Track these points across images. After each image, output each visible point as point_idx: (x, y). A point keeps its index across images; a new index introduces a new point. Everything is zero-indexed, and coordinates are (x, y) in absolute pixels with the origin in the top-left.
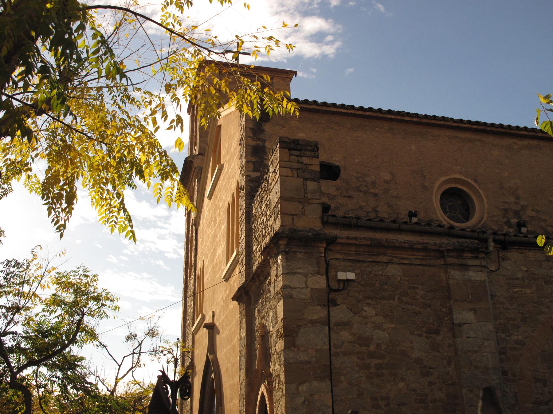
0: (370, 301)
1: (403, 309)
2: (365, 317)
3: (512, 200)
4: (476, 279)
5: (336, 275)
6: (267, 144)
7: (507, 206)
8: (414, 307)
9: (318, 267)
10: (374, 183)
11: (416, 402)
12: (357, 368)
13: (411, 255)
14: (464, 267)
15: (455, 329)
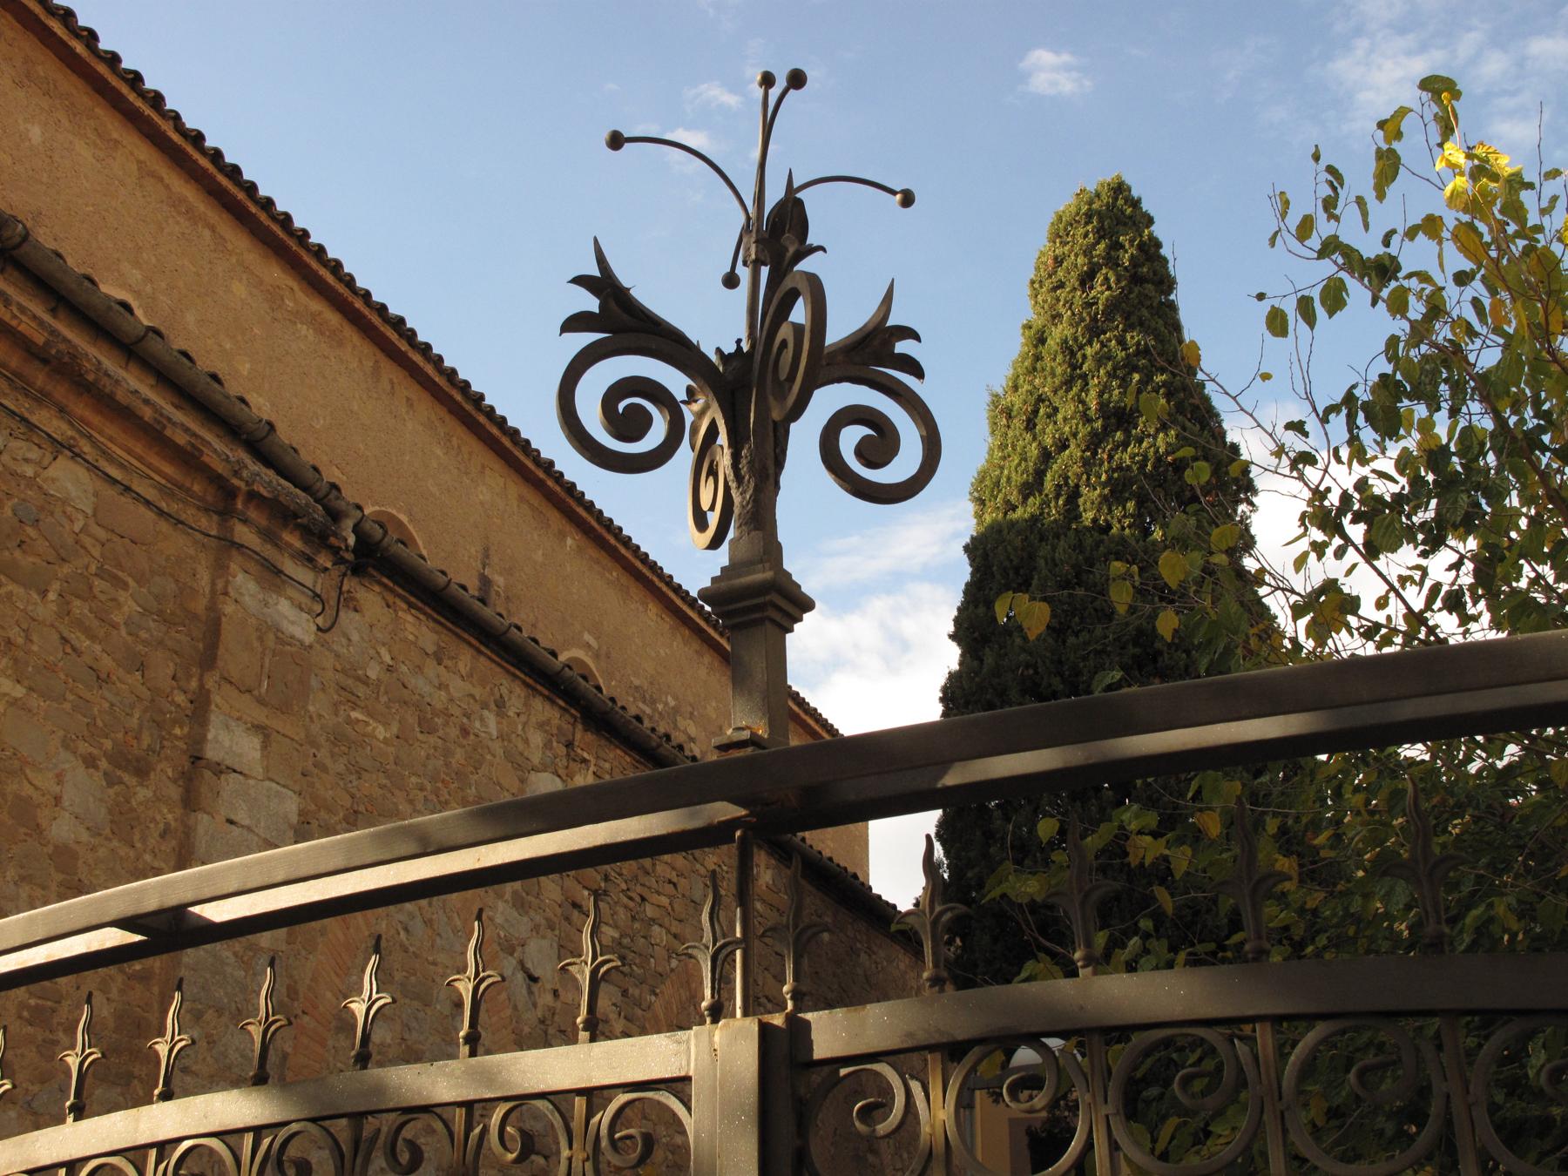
1: (65, 640)
8: (98, 648)
11: (20, 1017)
13: (140, 459)
14: (272, 575)
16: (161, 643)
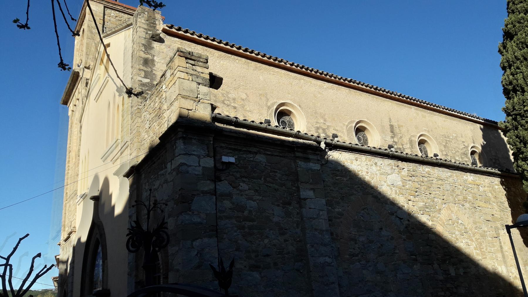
0: (244, 179)
1: (267, 186)
2: (241, 191)
3: (322, 121)
4: (314, 168)
5: (221, 158)
6: (155, 58)
7: (318, 125)
8: (274, 185)
9: (208, 151)
10: (234, 99)
12: (235, 229)
15: (301, 202)
16: (287, 180)
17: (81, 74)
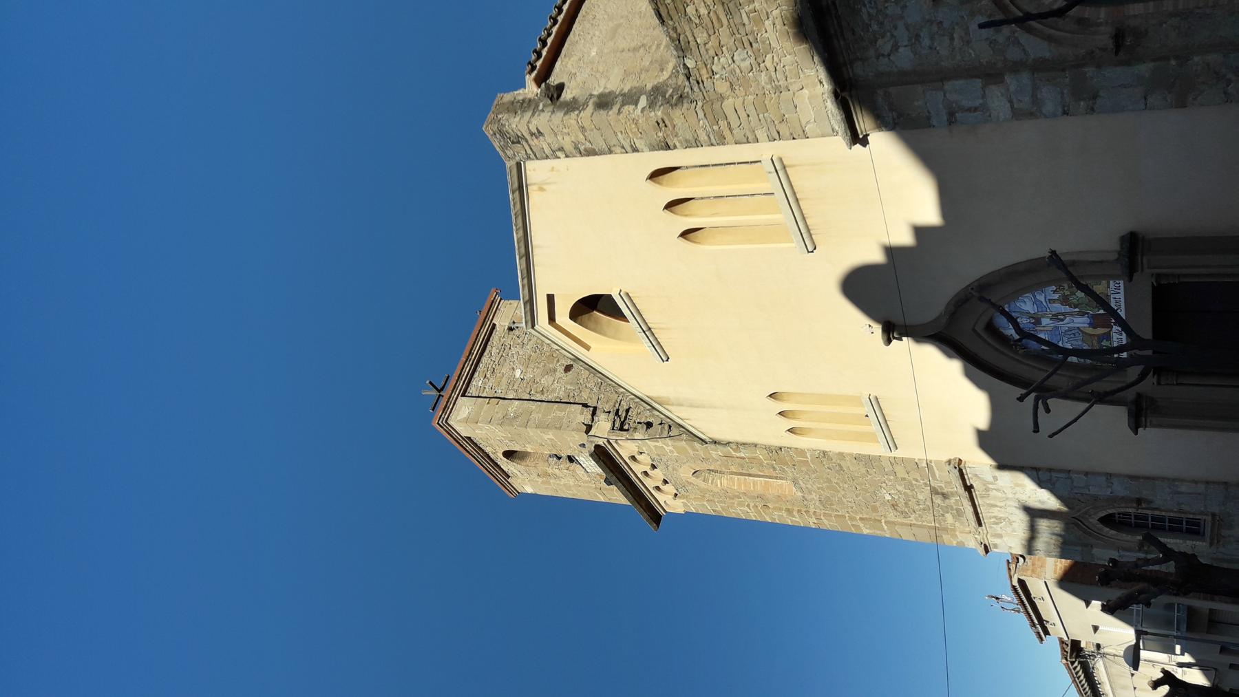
6: (595, 93)
17: (601, 442)
